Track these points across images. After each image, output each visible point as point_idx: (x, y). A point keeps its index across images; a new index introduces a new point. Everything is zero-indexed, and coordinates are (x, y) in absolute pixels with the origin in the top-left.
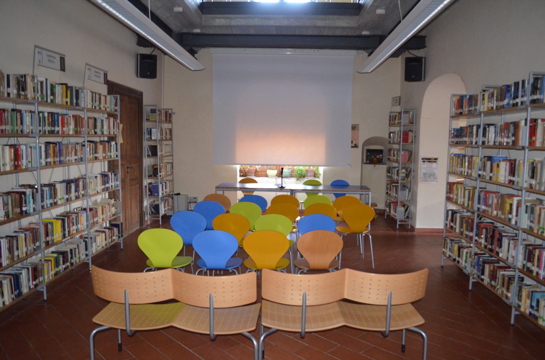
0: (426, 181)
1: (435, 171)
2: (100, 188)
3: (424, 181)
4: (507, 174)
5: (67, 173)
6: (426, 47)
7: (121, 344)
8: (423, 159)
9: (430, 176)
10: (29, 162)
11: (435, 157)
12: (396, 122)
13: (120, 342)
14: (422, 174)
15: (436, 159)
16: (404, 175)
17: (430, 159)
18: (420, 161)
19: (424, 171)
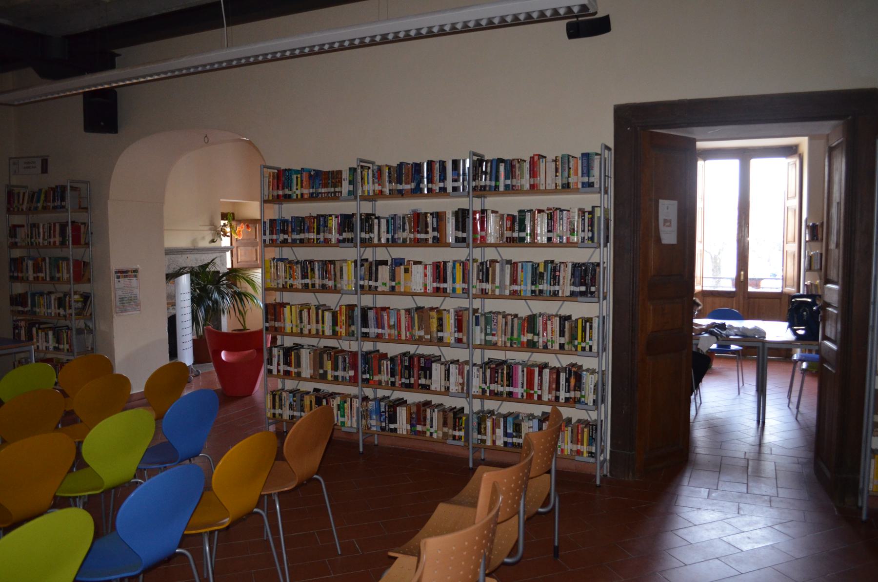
0: (125, 311)
1: (136, 291)
2: (279, 381)
3: (122, 312)
4: (430, 278)
5: (826, 200)
6: (116, 132)
7: (558, 547)
8: (117, 272)
9: (130, 302)
10: (497, 287)
11: (134, 267)
12: (40, 205)
13: (556, 544)
14: (117, 299)
15: (136, 271)
16: (80, 305)
17: (127, 272)
18: (113, 276)
19: (120, 293)
